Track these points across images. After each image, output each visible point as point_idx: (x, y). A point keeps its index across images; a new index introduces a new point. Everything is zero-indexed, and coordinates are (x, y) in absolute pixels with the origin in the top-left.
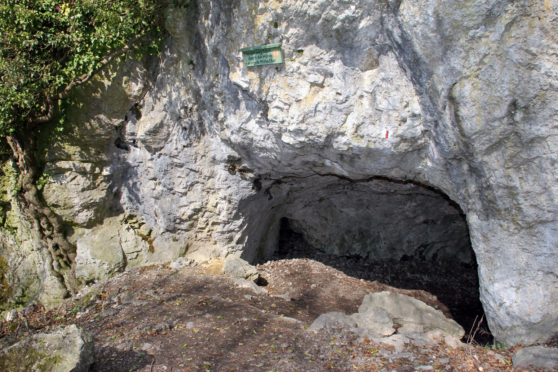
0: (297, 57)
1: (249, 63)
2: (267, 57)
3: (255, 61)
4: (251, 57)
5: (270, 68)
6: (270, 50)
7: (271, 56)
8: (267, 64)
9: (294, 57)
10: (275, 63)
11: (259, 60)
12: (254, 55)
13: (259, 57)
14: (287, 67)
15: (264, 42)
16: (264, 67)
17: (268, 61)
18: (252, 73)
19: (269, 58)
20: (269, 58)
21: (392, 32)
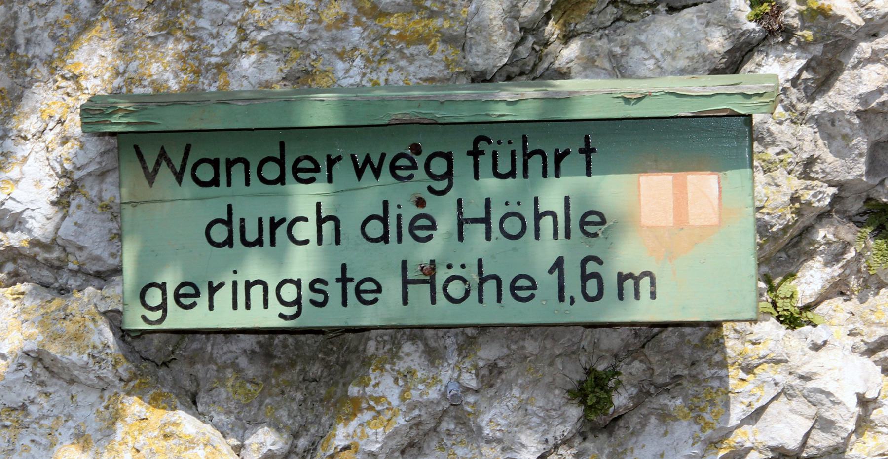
0: (837, 289)
1: (187, 293)
2: (523, 225)
3: (304, 262)
4: (252, 204)
5: (492, 376)
6: (588, 143)
7: (592, 222)
8: (513, 312)
9: (812, 278)
10: (644, 311)
11: (379, 262)
12: (305, 199)
13: (382, 226)
14: (745, 394)
15: (498, 48)
16: (411, 356)
17: (522, 288)
18: (186, 422)
19: (545, 250)
20: (545, 250)
21: (869, 326)
